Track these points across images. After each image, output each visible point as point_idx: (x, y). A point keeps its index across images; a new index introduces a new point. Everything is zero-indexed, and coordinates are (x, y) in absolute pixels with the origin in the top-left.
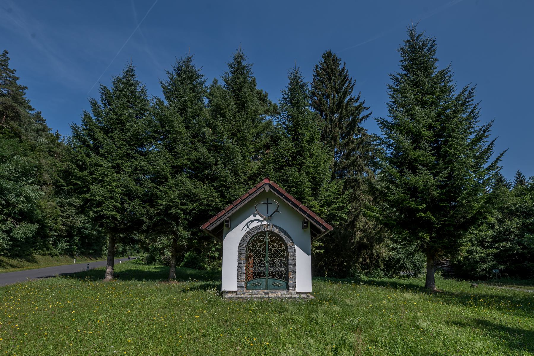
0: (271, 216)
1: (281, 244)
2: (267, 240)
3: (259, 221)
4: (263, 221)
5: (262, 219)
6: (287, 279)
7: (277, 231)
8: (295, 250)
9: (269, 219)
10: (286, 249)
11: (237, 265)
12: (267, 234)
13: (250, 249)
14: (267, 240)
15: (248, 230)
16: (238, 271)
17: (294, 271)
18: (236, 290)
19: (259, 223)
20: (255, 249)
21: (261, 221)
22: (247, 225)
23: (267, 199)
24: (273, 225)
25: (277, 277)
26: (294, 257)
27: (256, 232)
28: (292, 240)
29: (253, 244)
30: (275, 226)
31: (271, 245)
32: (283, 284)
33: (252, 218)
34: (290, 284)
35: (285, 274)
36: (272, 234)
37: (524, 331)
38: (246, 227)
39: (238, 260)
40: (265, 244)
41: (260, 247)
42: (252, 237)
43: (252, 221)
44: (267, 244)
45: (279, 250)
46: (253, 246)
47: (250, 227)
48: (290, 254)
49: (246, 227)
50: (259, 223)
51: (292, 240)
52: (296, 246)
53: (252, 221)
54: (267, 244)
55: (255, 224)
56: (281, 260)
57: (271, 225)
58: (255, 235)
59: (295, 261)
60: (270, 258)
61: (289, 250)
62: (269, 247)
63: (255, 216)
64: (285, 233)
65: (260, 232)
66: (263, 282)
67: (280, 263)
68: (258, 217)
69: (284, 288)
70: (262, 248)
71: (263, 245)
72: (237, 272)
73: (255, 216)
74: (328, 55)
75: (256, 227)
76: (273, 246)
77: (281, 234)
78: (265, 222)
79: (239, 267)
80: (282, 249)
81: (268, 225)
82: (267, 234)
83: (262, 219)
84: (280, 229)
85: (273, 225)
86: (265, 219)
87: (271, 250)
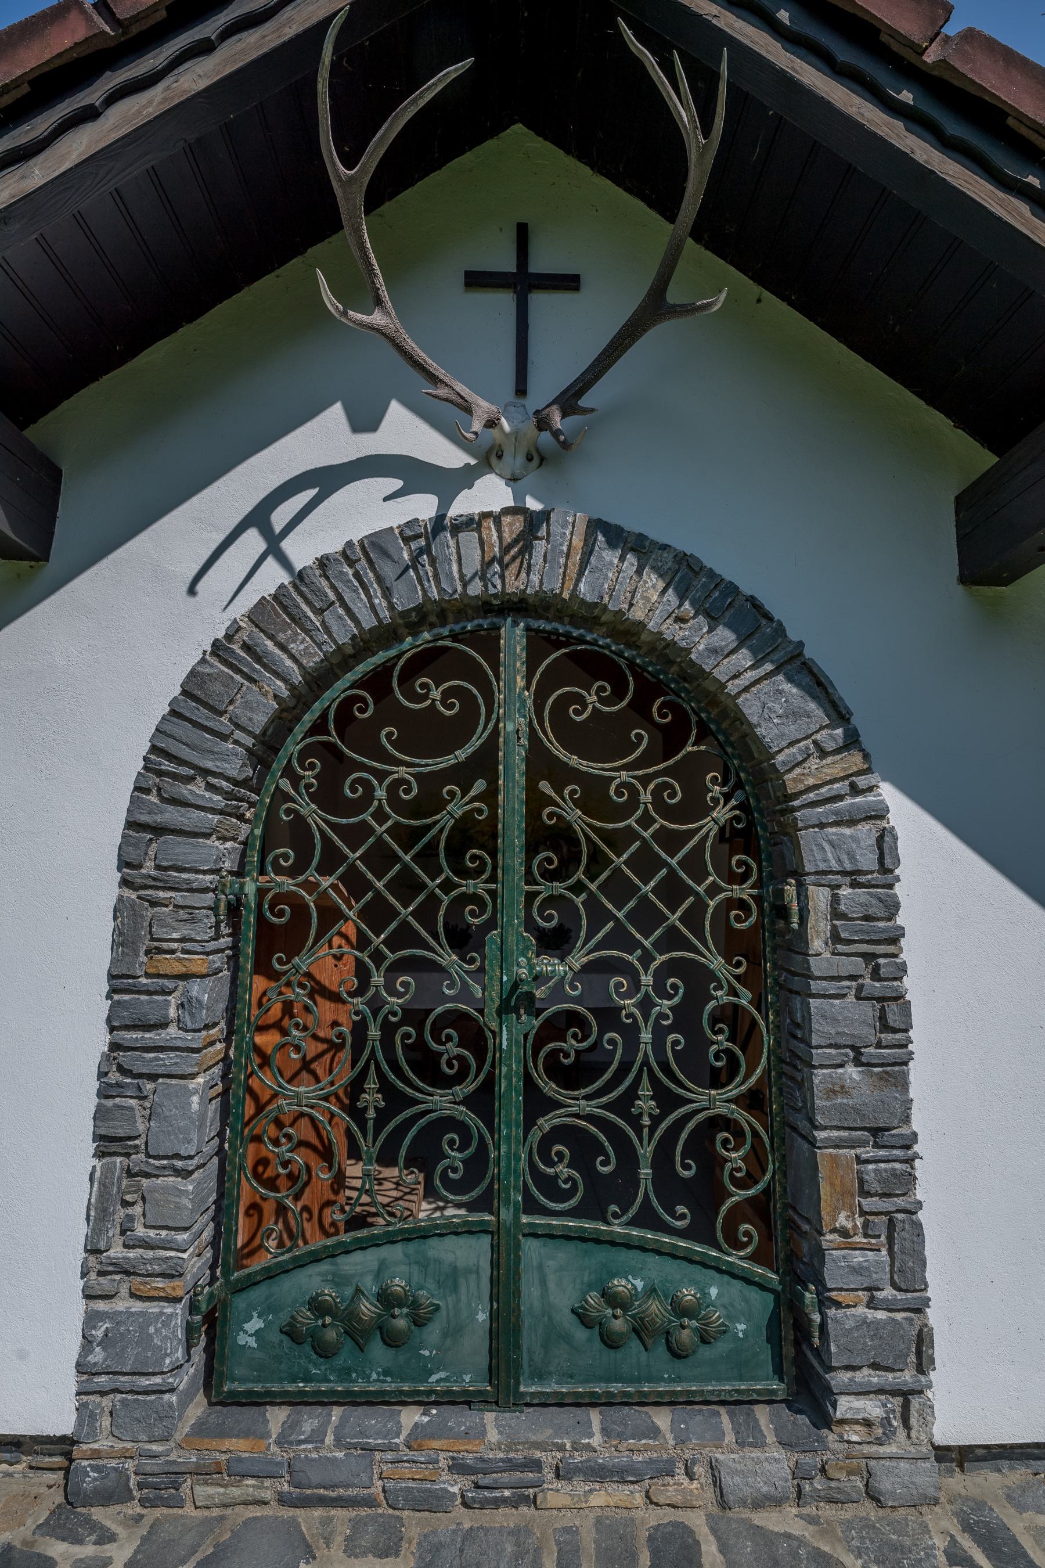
0: (569, 401)
1: (689, 773)
2: (514, 711)
3: (414, 474)
4: (466, 478)
5: (450, 456)
6: (785, 1242)
7: (648, 601)
8: (885, 844)
9: (537, 458)
10: (764, 835)
11: (100, 1040)
12: (514, 638)
13: (299, 832)
14: (514, 711)
15: (273, 577)
16: (107, 1144)
17: (889, 1135)
18: (61, 1421)
19: (423, 507)
20: (355, 835)
21: (446, 483)
22: (258, 518)
23: (523, 233)
24: (596, 525)
25: (646, 1219)
26: (879, 946)
27: (369, 610)
28: (839, 714)
29: (335, 765)
30: (616, 536)
31: (561, 775)
32: (731, 1302)
33: (325, 437)
34: (850, 1319)
35: (757, 1158)
36: (583, 648)
37: (896, 843)
38: (253, 542)
39: (118, 982)
40: (486, 762)
41: (430, 802)
42: (318, 680)
43: (327, 480)
44: (514, 760)
45: (671, 841)
46: (328, 796)
47: (304, 549)
48: (819, 897)
49: (253, 542)
50: (423, 507)
51: (839, 714)
52: (888, 793)
53: (327, 480)
54: (514, 760)
55: (367, 511)
56: (698, 979)
57: (568, 529)
58: (365, 644)
59: (891, 1015)
60: (556, 942)
61: (818, 849)
62: (535, 801)
63: (365, 421)
64: (752, 622)
65: (419, 618)
66: (452, 1278)
67: (686, 1017)
68: (404, 432)
69: (740, 1365)
70: (446, 820)
71: (462, 775)
72: (83, 1155)
73: (365, 421)
74: (110, 1558)
75: (375, 546)
76: (594, 797)
77: (706, 642)
78: (491, 494)
79: (124, 1074)
80: (709, 826)
81: (534, 522)
82: (514, 638)
83: (450, 456)
84: (685, 574)
85: (596, 525)
86: (489, 458)
87: (561, 838)
